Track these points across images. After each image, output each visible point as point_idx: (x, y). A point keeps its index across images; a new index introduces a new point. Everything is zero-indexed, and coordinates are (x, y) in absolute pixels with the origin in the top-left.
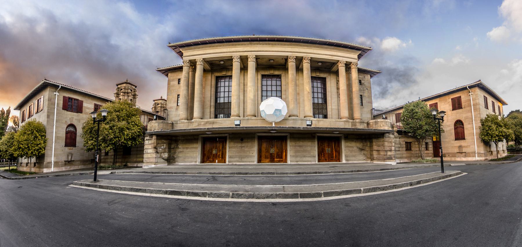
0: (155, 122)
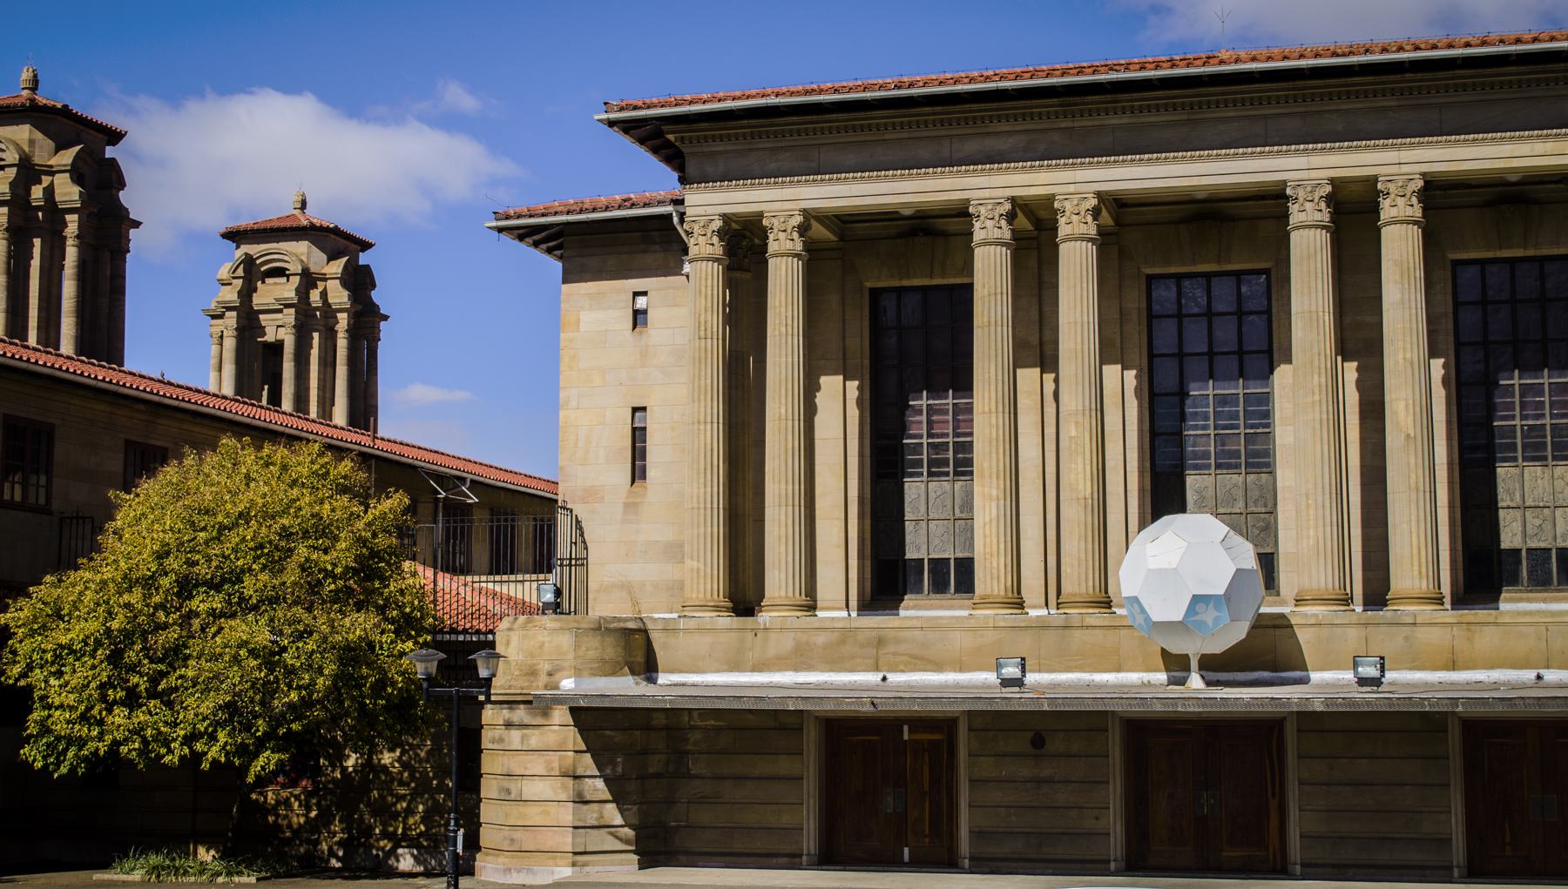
0: (557, 625)
